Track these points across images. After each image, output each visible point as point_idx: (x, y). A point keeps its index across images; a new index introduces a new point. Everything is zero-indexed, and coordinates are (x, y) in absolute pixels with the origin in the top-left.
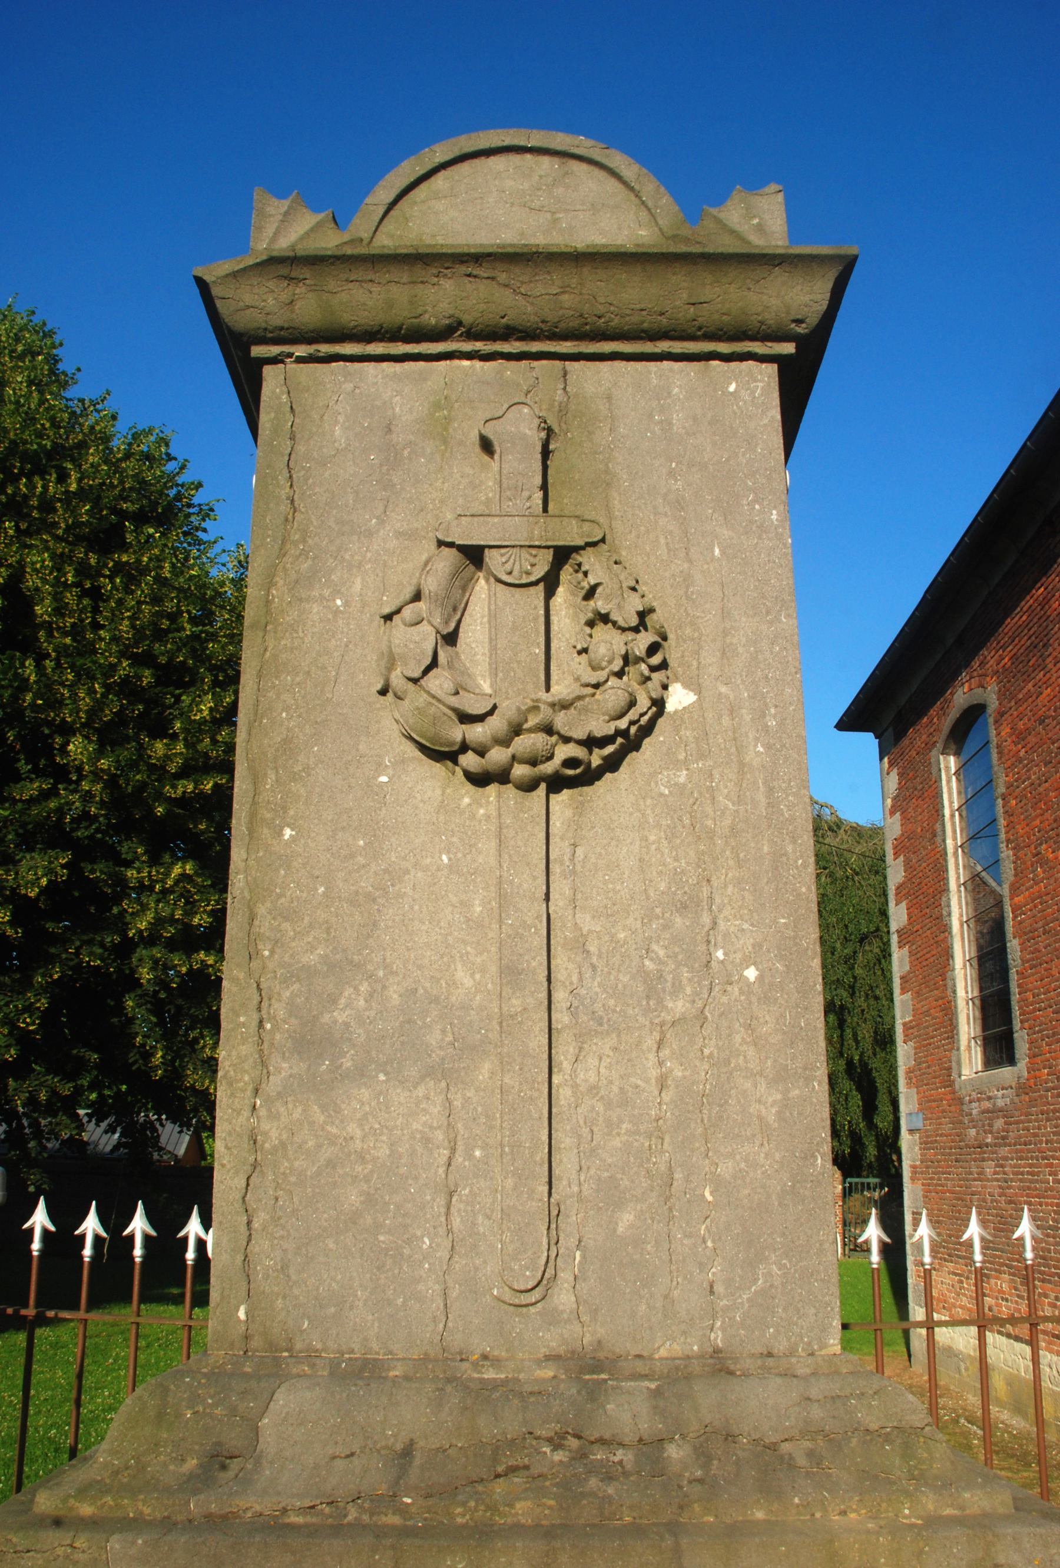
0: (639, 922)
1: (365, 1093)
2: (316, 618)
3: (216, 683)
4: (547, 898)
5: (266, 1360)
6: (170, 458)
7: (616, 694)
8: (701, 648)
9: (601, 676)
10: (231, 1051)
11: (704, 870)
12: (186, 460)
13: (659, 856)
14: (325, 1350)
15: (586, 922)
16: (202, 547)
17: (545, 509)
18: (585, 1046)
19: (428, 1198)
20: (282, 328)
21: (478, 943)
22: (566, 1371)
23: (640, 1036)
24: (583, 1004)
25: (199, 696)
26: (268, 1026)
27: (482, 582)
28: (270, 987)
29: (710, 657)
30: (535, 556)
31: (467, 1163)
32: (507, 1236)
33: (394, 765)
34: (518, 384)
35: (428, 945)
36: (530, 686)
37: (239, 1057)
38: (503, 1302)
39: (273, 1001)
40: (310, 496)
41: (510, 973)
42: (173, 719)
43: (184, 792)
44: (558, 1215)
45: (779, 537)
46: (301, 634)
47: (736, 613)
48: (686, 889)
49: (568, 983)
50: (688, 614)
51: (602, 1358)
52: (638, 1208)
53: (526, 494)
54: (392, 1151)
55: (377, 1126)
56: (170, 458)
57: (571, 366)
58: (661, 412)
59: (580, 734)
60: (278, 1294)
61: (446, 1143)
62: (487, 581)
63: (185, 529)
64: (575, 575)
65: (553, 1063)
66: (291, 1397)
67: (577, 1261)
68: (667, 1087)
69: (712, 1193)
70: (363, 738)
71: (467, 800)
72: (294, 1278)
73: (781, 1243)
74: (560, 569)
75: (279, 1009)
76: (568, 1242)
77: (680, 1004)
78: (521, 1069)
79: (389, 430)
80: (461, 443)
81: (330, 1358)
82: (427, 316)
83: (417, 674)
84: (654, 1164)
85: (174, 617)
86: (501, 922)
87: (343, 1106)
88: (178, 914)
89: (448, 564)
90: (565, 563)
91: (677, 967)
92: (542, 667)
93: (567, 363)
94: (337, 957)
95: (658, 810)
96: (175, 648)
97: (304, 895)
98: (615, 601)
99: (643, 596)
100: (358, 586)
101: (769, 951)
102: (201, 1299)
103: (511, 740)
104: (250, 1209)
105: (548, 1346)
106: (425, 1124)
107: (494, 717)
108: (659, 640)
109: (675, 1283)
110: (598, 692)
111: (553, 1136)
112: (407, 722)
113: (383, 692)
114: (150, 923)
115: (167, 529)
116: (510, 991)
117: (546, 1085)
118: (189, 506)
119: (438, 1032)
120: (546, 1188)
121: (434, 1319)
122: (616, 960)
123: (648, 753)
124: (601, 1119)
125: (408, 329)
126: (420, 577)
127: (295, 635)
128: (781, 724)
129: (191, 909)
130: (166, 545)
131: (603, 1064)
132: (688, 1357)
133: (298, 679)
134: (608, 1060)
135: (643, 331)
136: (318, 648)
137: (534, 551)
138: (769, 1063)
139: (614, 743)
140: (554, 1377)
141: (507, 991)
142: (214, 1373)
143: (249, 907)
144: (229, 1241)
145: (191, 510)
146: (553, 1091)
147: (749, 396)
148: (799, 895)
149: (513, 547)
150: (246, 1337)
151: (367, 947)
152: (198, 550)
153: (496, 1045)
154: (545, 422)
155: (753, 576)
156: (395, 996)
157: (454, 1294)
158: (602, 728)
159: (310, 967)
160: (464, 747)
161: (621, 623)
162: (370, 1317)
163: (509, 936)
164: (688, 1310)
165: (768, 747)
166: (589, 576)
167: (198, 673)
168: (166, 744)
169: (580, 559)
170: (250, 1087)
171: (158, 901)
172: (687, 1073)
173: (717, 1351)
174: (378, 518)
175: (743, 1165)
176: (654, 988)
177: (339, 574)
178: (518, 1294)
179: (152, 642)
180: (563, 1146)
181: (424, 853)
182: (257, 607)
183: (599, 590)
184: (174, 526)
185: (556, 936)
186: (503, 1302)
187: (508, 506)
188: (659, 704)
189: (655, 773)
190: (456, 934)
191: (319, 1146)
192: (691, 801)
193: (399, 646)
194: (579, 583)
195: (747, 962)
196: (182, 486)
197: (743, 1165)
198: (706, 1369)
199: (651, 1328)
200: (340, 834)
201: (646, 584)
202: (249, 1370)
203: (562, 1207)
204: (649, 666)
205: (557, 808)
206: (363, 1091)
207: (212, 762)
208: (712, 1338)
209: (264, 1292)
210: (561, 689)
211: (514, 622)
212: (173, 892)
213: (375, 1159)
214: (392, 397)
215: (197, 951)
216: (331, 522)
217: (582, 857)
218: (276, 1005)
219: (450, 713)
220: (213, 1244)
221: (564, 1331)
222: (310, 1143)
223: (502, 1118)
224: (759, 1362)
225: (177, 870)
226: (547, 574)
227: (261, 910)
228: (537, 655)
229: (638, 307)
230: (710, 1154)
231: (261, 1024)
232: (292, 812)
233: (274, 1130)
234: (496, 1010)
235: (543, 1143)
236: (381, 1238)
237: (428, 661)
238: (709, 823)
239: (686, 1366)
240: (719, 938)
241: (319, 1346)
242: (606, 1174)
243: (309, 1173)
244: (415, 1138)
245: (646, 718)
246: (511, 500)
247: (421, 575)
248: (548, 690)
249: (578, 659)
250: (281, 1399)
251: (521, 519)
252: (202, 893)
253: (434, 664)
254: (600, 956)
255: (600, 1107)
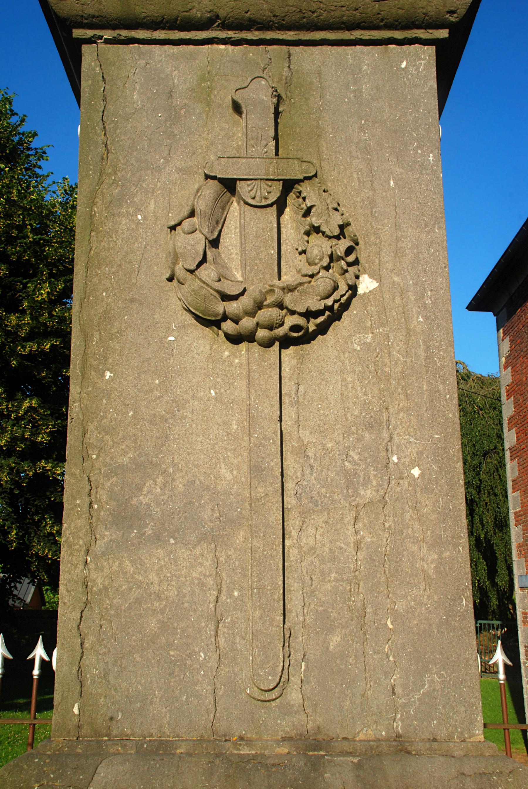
0: (341, 436)
1: (161, 552)
2: (124, 228)
3: (51, 275)
4: (281, 420)
5: (92, 743)
6: (13, 114)
7: (325, 282)
8: (381, 250)
9: (314, 269)
10: (70, 524)
11: (384, 402)
12: (25, 116)
13: (354, 392)
14: (133, 734)
15: (306, 436)
16: (38, 179)
17: (277, 154)
18: (306, 520)
19: (203, 624)
20: (94, 16)
21: (235, 450)
22: (297, 748)
23: (342, 514)
24: (305, 492)
25: (40, 284)
26: (96, 506)
27: (235, 204)
28: (96, 480)
29: (387, 257)
30: (271, 186)
31: (229, 600)
32: (256, 652)
33: (179, 329)
34: (258, 64)
35: (202, 451)
36: (268, 276)
37: (76, 528)
38: (254, 698)
39: (99, 489)
40: (118, 142)
41: (257, 471)
42: (22, 300)
43: (31, 351)
44: (290, 637)
45: (434, 172)
46: (115, 239)
47: (404, 226)
48: (372, 414)
49: (294, 477)
50: (372, 227)
51: (321, 739)
52: (343, 632)
53: (264, 142)
54: (179, 592)
55: (169, 575)
56: (13, 114)
57: (294, 50)
58: (355, 84)
59: (301, 309)
60: (101, 694)
61: (215, 587)
62: (238, 203)
63: (26, 165)
64: (297, 200)
65: (285, 532)
66: (109, 770)
67: (302, 670)
68: (361, 549)
69: (392, 623)
70: (157, 310)
71: (227, 353)
72: (112, 682)
73: (439, 659)
74: (287, 196)
75: (103, 495)
76: (297, 656)
77: (369, 492)
78: (264, 536)
79: (171, 96)
80: (219, 106)
81: (136, 741)
82: (194, 11)
83: (193, 267)
84: (353, 601)
85: (21, 228)
86: (250, 436)
87: (146, 561)
88: (27, 435)
89: (212, 191)
90: (291, 191)
91: (367, 467)
92: (276, 263)
93: (290, 47)
94: (142, 459)
95: (353, 361)
96: (22, 250)
97: (120, 417)
98: (324, 218)
99: (342, 215)
100: (152, 206)
101: (427, 457)
102: (46, 705)
103: (256, 312)
104: (82, 634)
105: (284, 730)
106: (201, 573)
107: (245, 296)
108: (354, 245)
109: (368, 686)
110: (313, 280)
111: (286, 582)
112: (187, 300)
113: (170, 279)
114: (7, 441)
115: (13, 165)
116: (257, 482)
117: (281, 547)
118: (29, 149)
119: (209, 510)
120: (282, 618)
121: (208, 711)
122: (326, 462)
123: (346, 322)
124: (317, 570)
125: (182, 21)
126: (194, 200)
127: (111, 239)
128: (435, 302)
129: (36, 431)
130: (13, 177)
131: (318, 533)
132: (379, 740)
133: (113, 270)
134: (322, 530)
135: (343, 23)
136: (126, 248)
137: (270, 183)
138: (429, 533)
139: (324, 315)
140: (289, 753)
141: (255, 483)
142: (56, 754)
143: (82, 425)
144: (68, 657)
145: (30, 153)
146: (286, 551)
147: (415, 71)
148: (447, 419)
149: (256, 180)
150: (79, 727)
151: (161, 452)
152: (36, 181)
153: (248, 519)
154: (276, 91)
155: (416, 201)
156: (181, 486)
157: (220, 692)
158: (316, 305)
159: (124, 466)
160: (225, 317)
161: (328, 233)
162: (164, 710)
163: (256, 445)
164: (377, 706)
165: (426, 318)
166: (307, 200)
167: (39, 268)
168: (18, 317)
169: (300, 188)
170: (84, 549)
171: (13, 425)
172: (374, 540)
173: (398, 736)
174: (164, 158)
175: (412, 604)
176: (351, 481)
177: (139, 198)
178: (264, 693)
179: (6, 245)
180: (292, 589)
181: (199, 389)
182: (85, 219)
183: (313, 210)
184: (18, 163)
185: (287, 446)
186: (254, 698)
187: (252, 151)
188: (353, 288)
189: (349, 337)
190: (221, 443)
191: (130, 589)
192: (375, 354)
193: (181, 247)
194: (300, 205)
195: (413, 464)
196: (23, 134)
197: (412, 604)
198: (391, 749)
199: (353, 718)
200: (143, 376)
201: (344, 206)
202: (80, 751)
203: (292, 631)
204: (346, 262)
205: (287, 359)
206: (159, 550)
207: (49, 329)
208: (395, 727)
209: (91, 693)
210: (289, 277)
211: (257, 232)
212: (24, 419)
213: (167, 598)
214: (172, 71)
215: (40, 461)
216: (133, 161)
217: (303, 392)
218: (101, 492)
219: (215, 294)
220: (57, 659)
221: (295, 719)
222: (124, 587)
223: (252, 569)
224: (428, 745)
225: (26, 404)
226: (279, 198)
227: (91, 427)
228: (272, 254)
229: (340, 4)
230: (391, 595)
231: (91, 505)
232: (110, 361)
233: (99, 578)
234: (247, 495)
235: (279, 587)
236: (172, 653)
237: (200, 258)
238: (387, 369)
239: (377, 747)
240: (394, 448)
241: (129, 732)
242: (321, 608)
243: (123, 608)
244: (194, 583)
245: (345, 298)
246: (254, 147)
247: (194, 199)
248: (280, 279)
249: (299, 257)
250: (102, 772)
251: (260, 160)
252: (44, 419)
253: (204, 260)
254: (315, 459)
255: (317, 562)
